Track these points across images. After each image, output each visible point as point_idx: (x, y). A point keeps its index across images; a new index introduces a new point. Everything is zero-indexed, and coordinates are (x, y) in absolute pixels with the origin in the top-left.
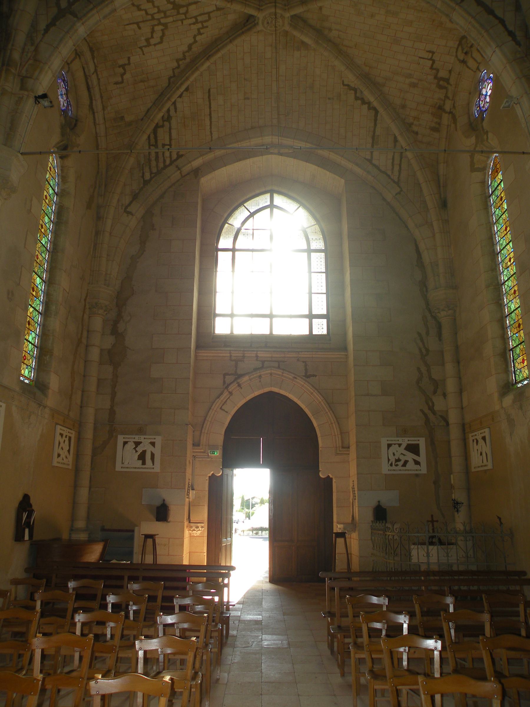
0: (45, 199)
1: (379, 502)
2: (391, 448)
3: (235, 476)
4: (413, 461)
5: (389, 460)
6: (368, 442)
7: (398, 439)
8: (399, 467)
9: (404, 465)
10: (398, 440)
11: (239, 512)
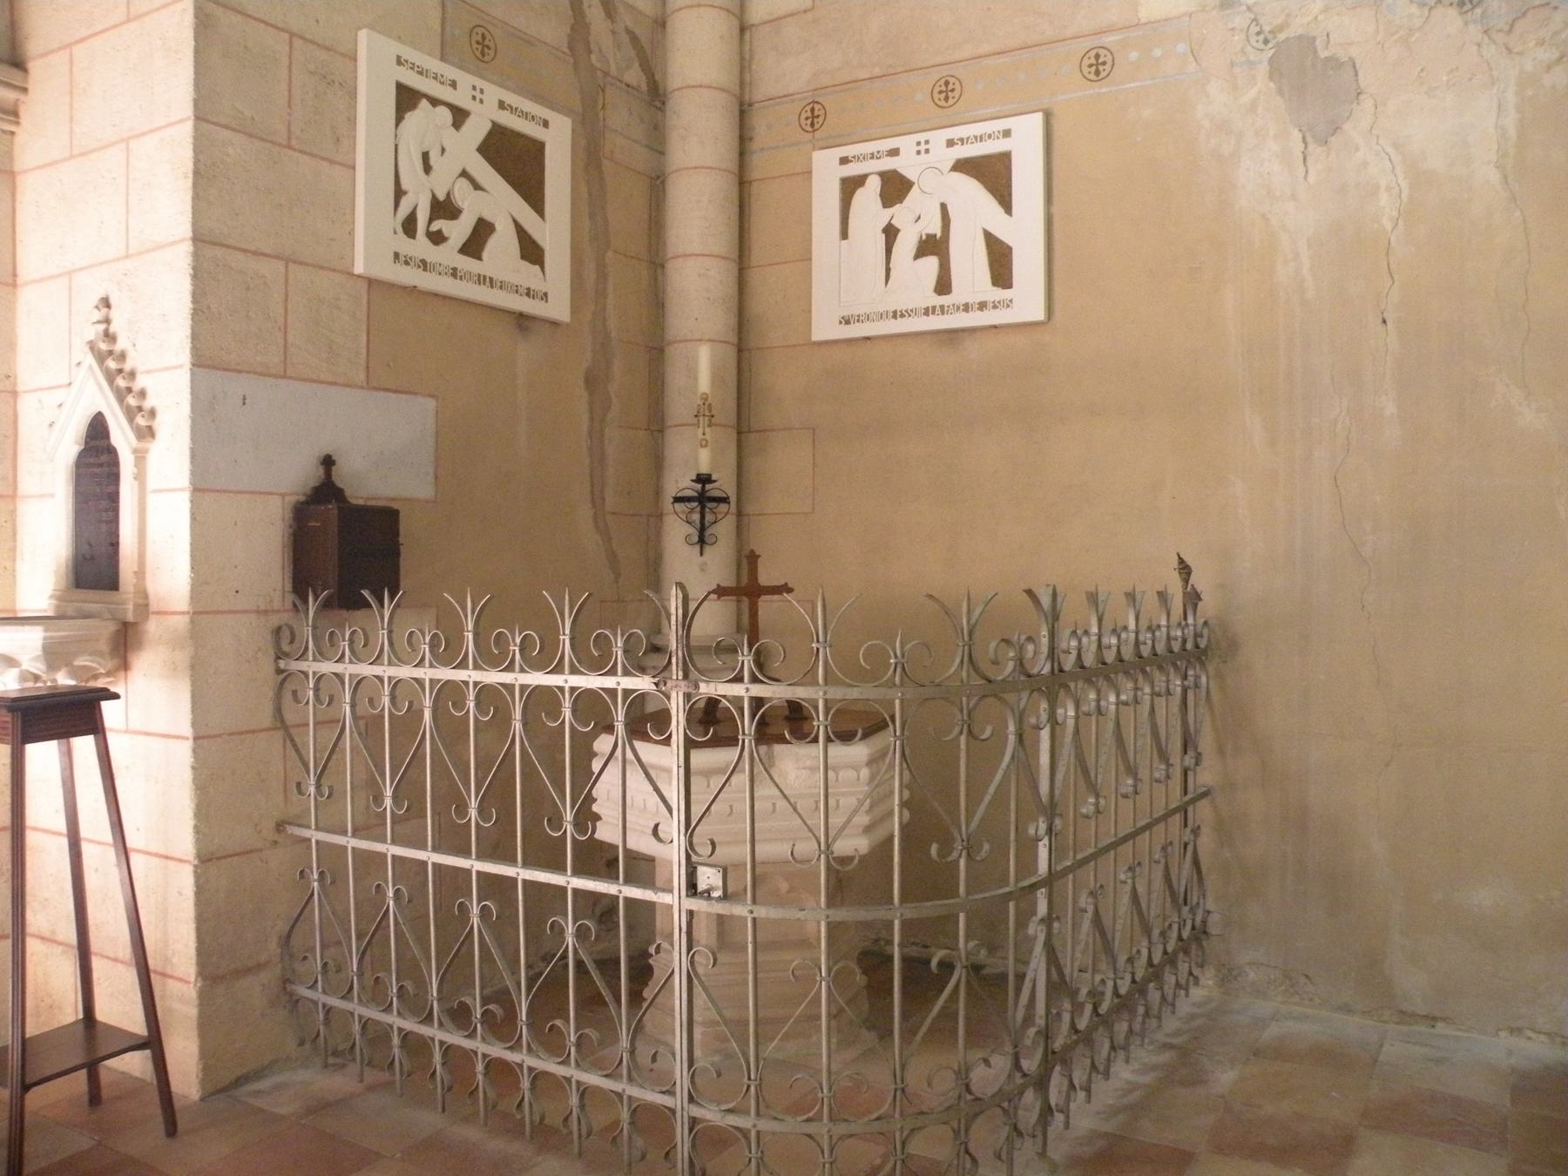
0: (330, 1053)
1: (328, 462)
2: (413, 119)
3: (295, 605)
4: (514, 229)
5: (399, 193)
6: (282, 30)
7: (452, 77)
8: (448, 254)
9: (474, 245)
10: (454, 85)
11: (113, 308)
